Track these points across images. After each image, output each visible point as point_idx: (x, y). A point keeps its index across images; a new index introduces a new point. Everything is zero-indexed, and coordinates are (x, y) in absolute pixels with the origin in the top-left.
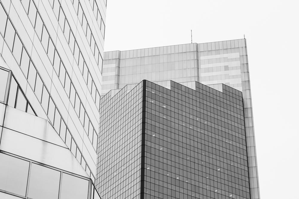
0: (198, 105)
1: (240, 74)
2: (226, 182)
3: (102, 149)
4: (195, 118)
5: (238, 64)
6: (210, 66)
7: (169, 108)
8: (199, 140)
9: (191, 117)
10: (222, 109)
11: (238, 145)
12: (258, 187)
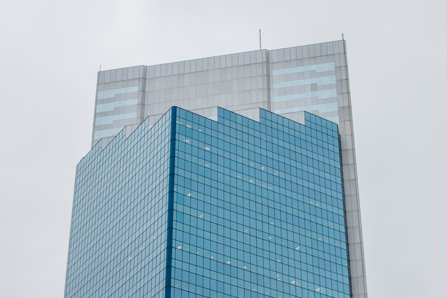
0: (264, 146)
1: (336, 95)
2: (310, 268)
3: (124, 224)
4: (258, 166)
5: (331, 80)
6: (288, 84)
7: (214, 150)
8: (265, 202)
9: (252, 164)
10: (310, 154)
11: (330, 208)
12: (364, 276)
